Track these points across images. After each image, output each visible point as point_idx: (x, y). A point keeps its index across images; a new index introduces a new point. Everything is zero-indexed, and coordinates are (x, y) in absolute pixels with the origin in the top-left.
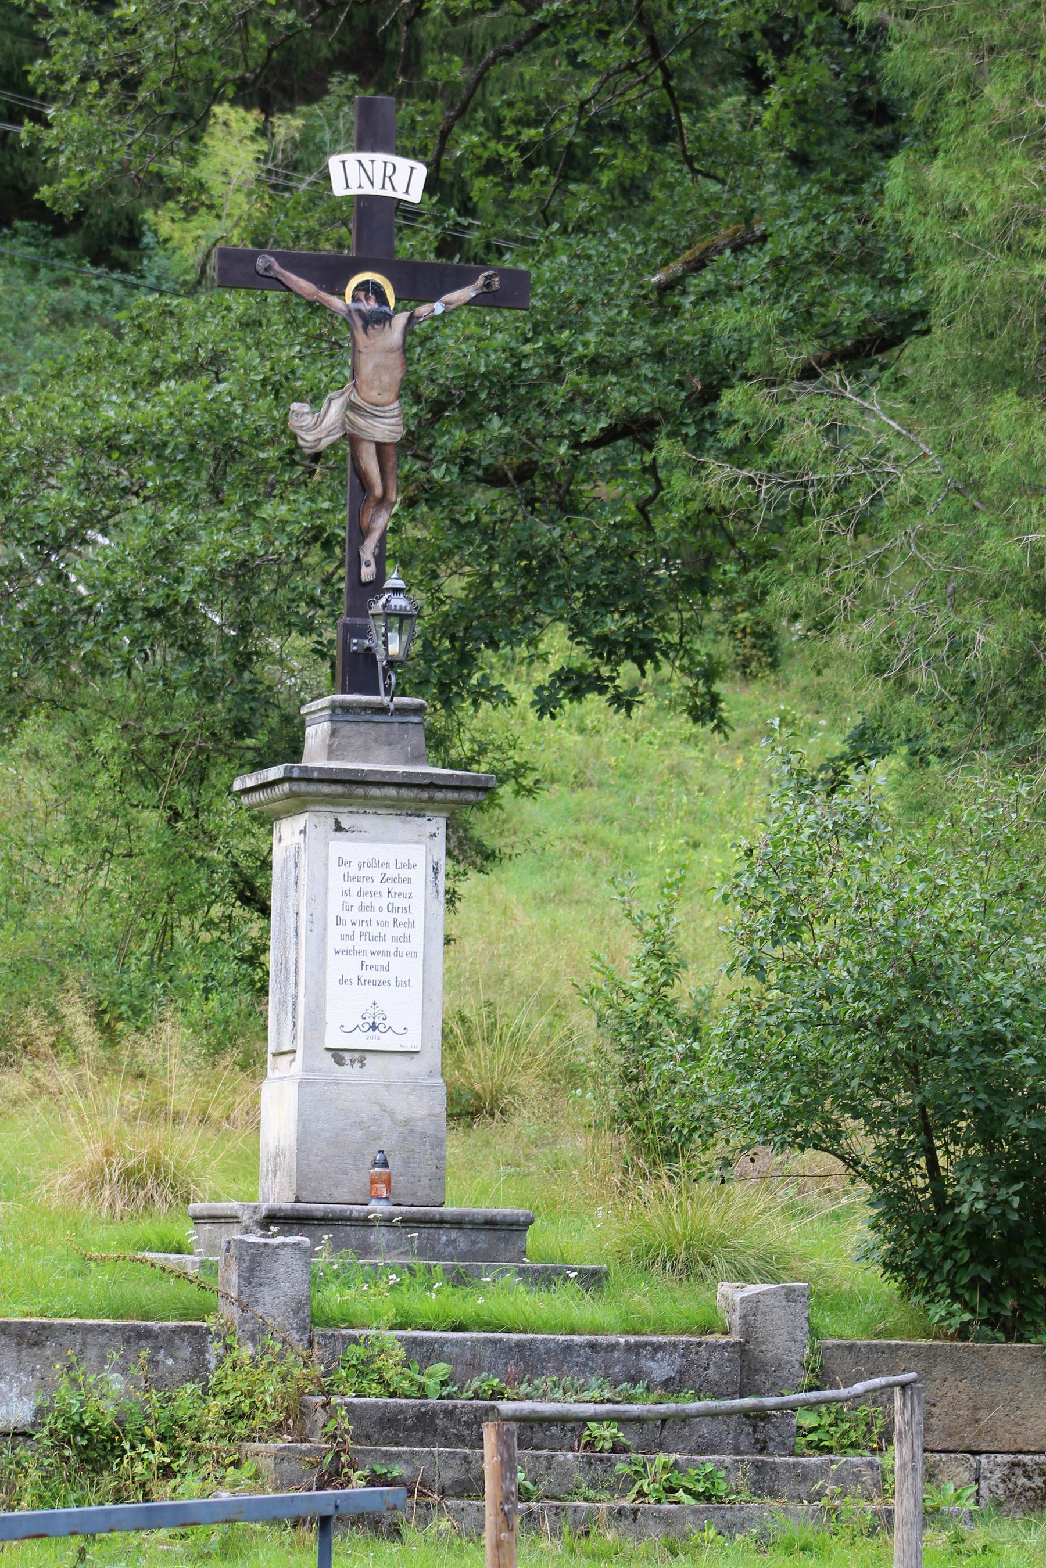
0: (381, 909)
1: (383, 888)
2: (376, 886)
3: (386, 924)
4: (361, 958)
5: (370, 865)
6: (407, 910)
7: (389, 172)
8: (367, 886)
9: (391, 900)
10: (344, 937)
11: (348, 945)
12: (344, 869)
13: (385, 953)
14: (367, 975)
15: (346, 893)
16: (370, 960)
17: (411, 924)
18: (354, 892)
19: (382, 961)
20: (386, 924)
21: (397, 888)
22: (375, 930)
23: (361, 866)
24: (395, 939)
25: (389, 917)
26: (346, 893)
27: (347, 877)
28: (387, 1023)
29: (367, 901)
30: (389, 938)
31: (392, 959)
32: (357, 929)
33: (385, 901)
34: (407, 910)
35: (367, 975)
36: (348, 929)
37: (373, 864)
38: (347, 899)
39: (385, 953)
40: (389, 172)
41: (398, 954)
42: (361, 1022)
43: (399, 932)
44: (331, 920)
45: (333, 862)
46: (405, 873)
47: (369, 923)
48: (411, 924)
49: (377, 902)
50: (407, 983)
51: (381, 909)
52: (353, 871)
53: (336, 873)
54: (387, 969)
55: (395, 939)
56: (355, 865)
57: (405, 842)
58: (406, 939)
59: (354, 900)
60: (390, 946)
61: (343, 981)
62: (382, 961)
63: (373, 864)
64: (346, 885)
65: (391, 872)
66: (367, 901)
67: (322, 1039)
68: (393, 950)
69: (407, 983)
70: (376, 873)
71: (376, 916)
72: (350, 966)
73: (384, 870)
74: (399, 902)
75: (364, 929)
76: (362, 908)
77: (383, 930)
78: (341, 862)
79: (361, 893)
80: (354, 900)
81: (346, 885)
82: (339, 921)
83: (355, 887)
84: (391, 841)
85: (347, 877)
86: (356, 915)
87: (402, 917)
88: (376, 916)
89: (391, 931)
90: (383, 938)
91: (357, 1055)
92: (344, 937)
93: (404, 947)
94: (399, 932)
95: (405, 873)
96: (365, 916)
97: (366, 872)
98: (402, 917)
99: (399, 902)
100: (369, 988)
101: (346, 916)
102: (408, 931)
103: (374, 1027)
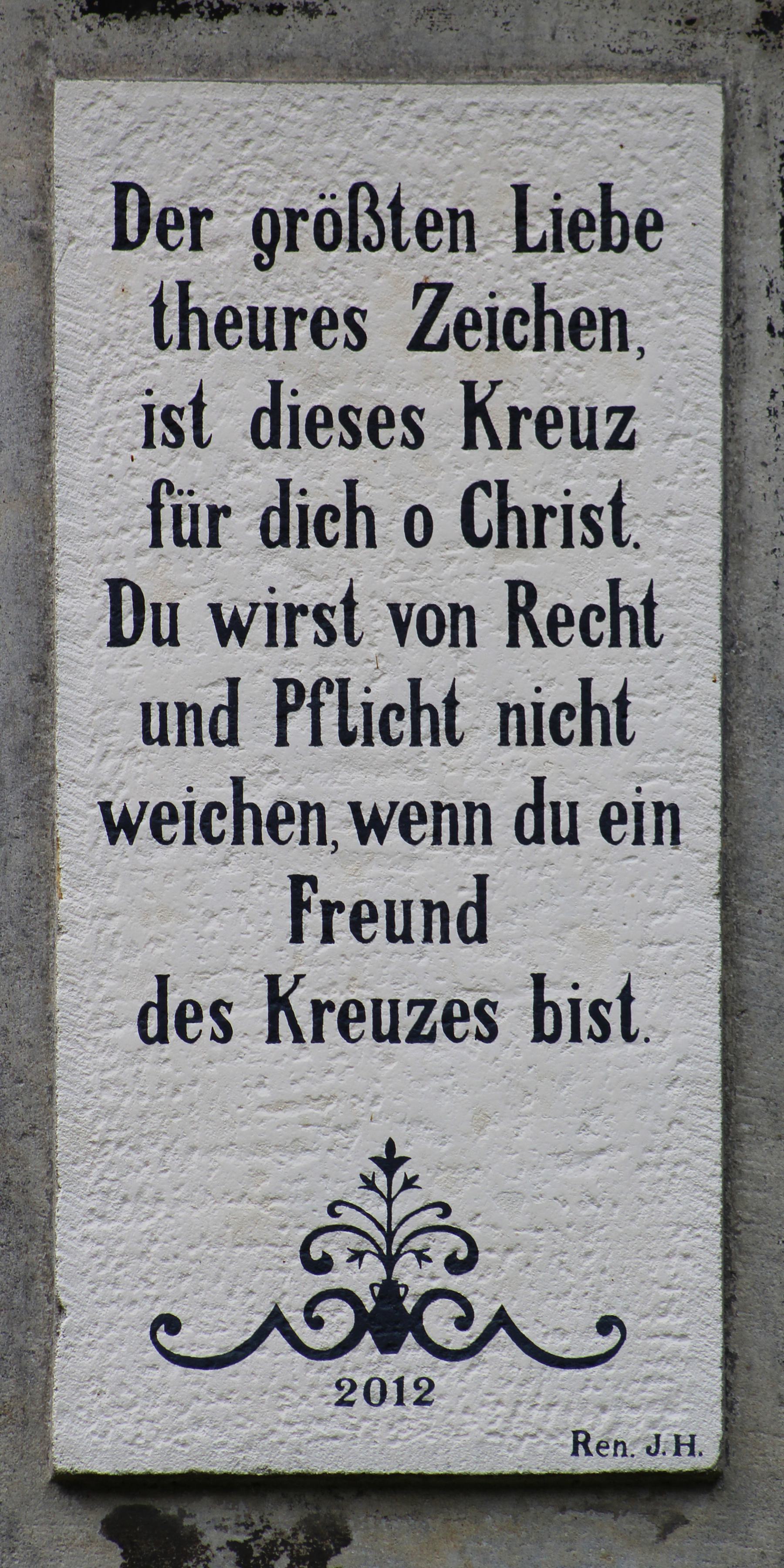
0: (418, 527)
1: (435, 385)
2: (387, 373)
3: (451, 624)
4: (278, 861)
5: (337, 233)
6: (601, 524)
7: (522, 601)
8: (320, 377)
9: (488, 464)
10: (161, 724)
11: (197, 774)
12: (155, 266)
13: (459, 822)
14: (336, 969)
15: (175, 424)
16: (353, 873)
17: (634, 621)
18: (227, 422)
19: (437, 872)
20: (451, 624)
21: (530, 378)
22: (380, 669)
23: (272, 236)
24: (521, 724)
25: (477, 579)
26: (175, 424)
27: (180, 321)
28: (482, 1289)
29: (320, 473)
30: (477, 718)
31: (502, 857)
32: (258, 665)
33: (443, 471)
34: (601, 524)
35: (336, 969)
36: (193, 669)
37: (359, 221)
38: (182, 466)
39: (459, 822)
40: (522, 601)
41: (544, 821)
42: (296, 1288)
43: (554, 673)
44: (80, 607)
45: (82, 212)
46: (579, 279)
47: (337, 622)
48: (634, 621)
49: (387, 478)
50: (611, 1019)
51: (418, 527)
52: (223, 273)
53: (101, 295)
54: (470, 921)
55: (521, 724)
56: (230, 229)
57: (588, 69)
58: (602, 720)
59: (235, 474)
60: (487, 771)
61: (165, 1019)
62: (437, 872)
63: (359, 221)
64: (174, 376)
65: (493, 274)
66: (320, 473)
67: (30, 1414)
68: (507, 795)
69: (611, 1019)
70: (381, 283)
71: (385, 573)
72: (217, 918)
73: (439, 265)
74: (538, 474)
75: (307, 662)
76: (288, 523)
77: (438, 667)
78: (137, 218)
79: (277, 424)
80: (235, 474)
81: (174, 376)
82: (134, 617)
83: (235, 381)
84: (489, 69)
85: (180, 321)
86: (244, 569)
87: (569, 576)
88: (385, 573)
89: (492, 672)
90: (435, 721)
91: (284, 1519)
92: (161, 724)
93: (583, 775)
94: (554, 673)
95: (579, 279)
96: (311, 575)
97: (308, 277)
98: (569, 576)
99: (538, 474)
100: (362, 1060)
101: (184, 580)
102: (610, 668)
103: (389, 1320)
